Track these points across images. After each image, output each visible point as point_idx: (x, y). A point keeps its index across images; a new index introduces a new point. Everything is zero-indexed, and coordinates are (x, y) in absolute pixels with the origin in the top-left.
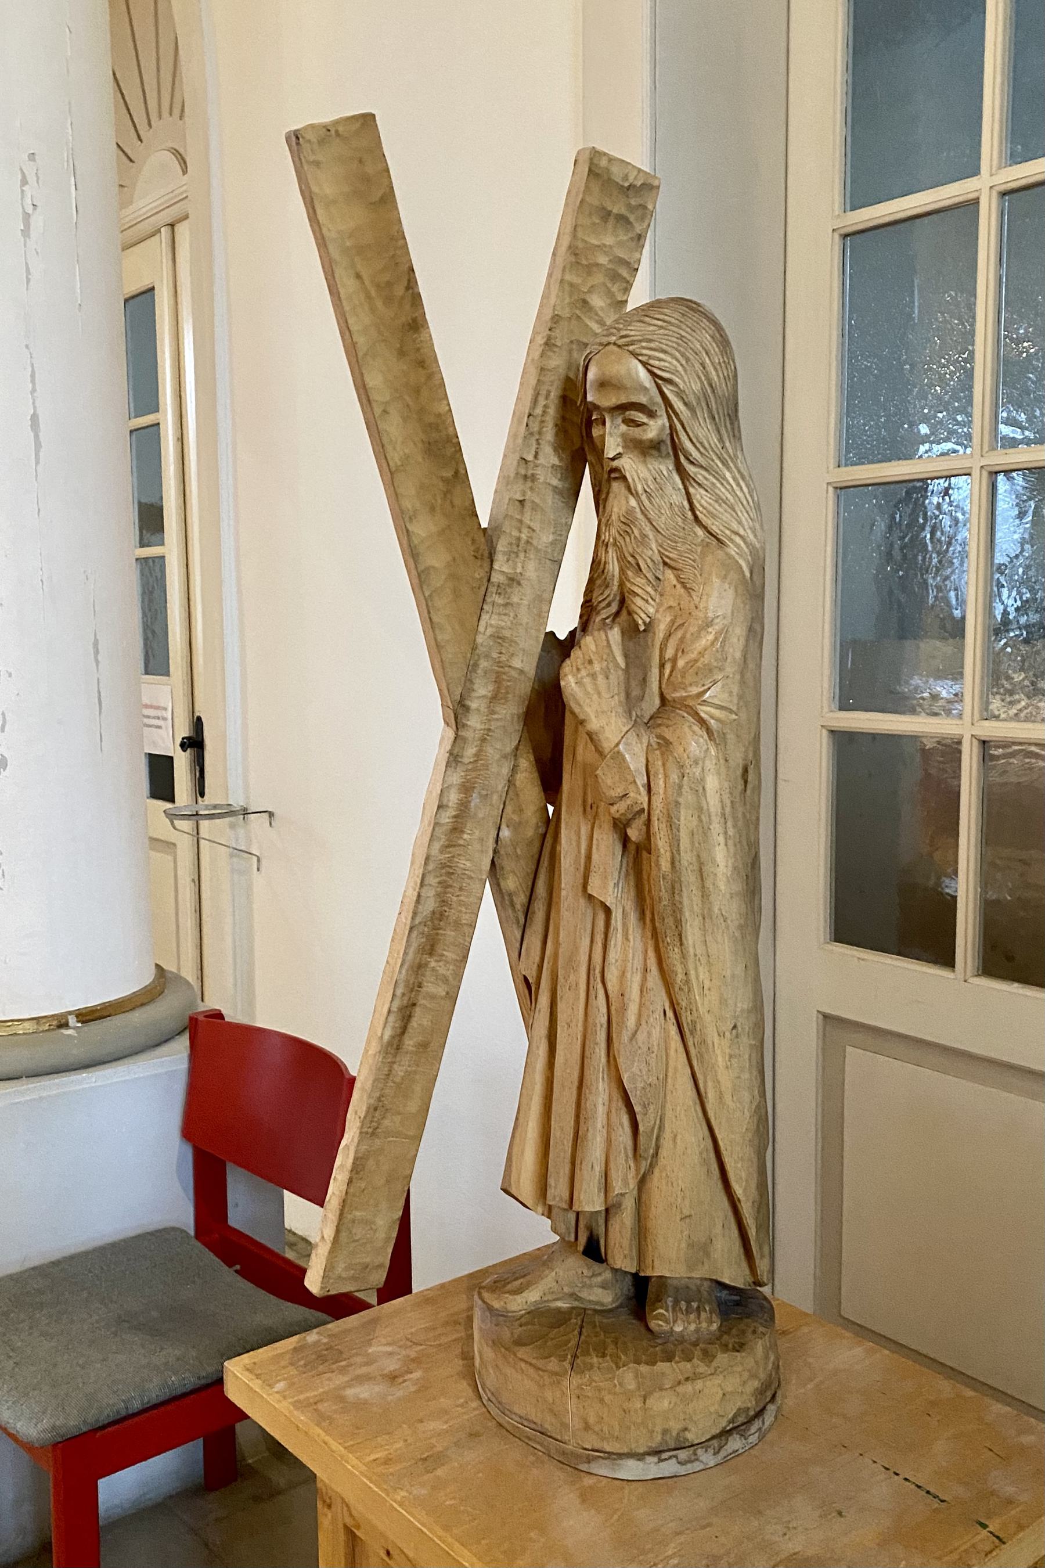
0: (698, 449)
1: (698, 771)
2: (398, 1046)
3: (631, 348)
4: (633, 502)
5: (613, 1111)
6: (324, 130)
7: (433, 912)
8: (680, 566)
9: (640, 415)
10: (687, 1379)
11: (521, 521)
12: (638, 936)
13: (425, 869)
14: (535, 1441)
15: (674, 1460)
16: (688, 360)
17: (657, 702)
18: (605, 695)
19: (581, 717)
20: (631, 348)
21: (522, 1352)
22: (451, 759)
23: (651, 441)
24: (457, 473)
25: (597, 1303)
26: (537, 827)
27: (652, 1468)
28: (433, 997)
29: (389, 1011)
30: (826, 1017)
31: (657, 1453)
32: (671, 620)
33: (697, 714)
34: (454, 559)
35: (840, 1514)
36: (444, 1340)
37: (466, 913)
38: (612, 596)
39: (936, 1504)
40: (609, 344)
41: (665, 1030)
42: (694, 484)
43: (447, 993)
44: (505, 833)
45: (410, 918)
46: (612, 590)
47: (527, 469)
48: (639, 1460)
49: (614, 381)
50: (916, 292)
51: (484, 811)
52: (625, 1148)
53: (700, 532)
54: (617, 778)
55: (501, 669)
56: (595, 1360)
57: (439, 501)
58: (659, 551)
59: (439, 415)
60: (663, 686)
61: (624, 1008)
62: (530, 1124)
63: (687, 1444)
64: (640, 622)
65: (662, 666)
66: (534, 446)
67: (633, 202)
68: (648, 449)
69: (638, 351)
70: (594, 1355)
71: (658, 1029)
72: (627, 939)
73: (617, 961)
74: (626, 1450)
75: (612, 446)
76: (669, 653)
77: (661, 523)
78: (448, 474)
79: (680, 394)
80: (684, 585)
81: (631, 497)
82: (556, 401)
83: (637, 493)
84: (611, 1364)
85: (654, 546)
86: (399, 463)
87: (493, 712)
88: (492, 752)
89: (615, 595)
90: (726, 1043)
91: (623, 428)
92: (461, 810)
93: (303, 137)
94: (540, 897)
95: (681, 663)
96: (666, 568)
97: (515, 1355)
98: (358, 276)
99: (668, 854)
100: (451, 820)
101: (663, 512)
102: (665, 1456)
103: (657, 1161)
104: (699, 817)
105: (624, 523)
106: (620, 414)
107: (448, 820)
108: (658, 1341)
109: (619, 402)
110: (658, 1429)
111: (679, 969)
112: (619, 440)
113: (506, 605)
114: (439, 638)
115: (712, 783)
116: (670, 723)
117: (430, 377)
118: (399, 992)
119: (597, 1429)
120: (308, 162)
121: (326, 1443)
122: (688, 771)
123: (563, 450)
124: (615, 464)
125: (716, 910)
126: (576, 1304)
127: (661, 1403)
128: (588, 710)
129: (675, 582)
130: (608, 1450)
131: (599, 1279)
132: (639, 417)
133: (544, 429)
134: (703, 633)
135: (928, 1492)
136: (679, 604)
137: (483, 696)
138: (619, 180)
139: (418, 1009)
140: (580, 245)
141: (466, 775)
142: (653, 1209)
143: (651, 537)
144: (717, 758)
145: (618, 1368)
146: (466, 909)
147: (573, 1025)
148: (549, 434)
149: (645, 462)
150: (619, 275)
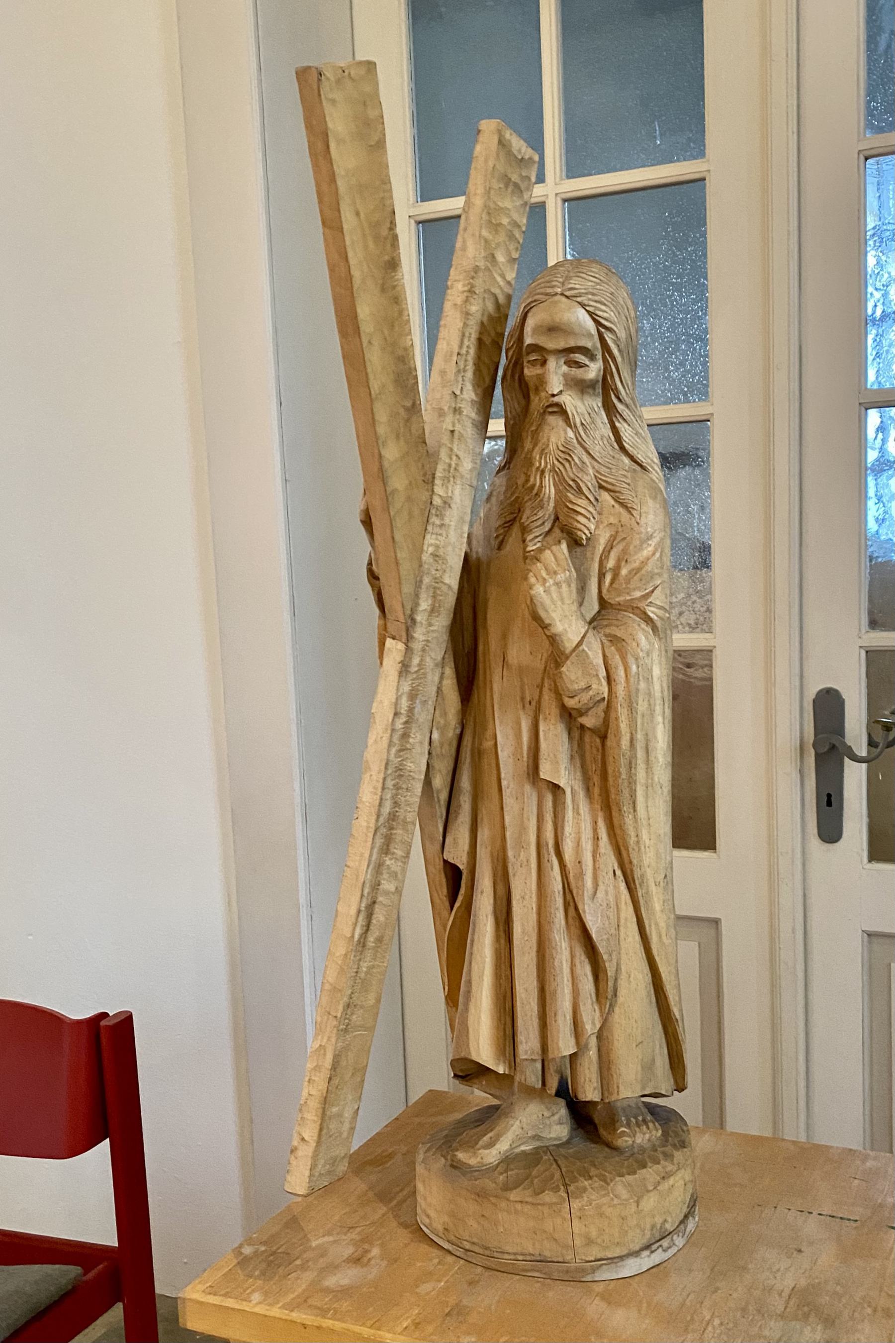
0: (625, 390)
1: (648, 661)
2: (364, 943)
3: (579, 299)
4: (571, 434)
5: (578, 964)
6: (341, 71)
7: (390, 814)
8: (617, 489)
9: (583, 357)
10: (663, 1178)
11: (451, 450)
12: (586, 809)
13: (385, 773)
15: (660, 1250)
16: (619, 313)
17: (596, 607)
18: (567, 601)
19: (547, 621)
20: (579, 299)
21: (513, 1195)
22: (403, 669)
23: (591, 380)
24: (414, 404)
25: (555, 1139)
26: (456, 728)
27: (646, 1261)
28: (387, 893)
29: (359, 911)
31: (647, 1247)
32: (611, 536)
33: (645, 613)
34: (410, 482)
35: (800, 1251)
36: (377, 1217)
37: (410, 812)
38: (547, 516)
39: (854, 1225)
40: (556, 294)
41: (616, 887)
42: (620, 420)
43: (397, 888)
44: (436, 736)
45: (373, 821)
46: (547, 510)
47: (456, 403)
48: (636, 1257)
49: (563, 327)
51: (423, 716)
52: (591, 995)
53: (626, 460)
54: (580, 673)
55: (436, 585)
56: (586, 1183)
57: (402, 429)
58: (595, 475)
59: (406, 349)
60: (604, 591)
61: (581, 875)
62: (484, 993)
63: (667, 1233)
64: (584, 537)
65: (601, 576)
66: (461, 382)
67: (524, 174)
68: (583, 387)
69: (586, 302)
70: (582, 1179)
71: (612, 887)
72: (578, 814)
73: (570, 834)
74: (625, 1252)
75: (555, 384)
76: (611, 563)
77: (596, 451)
78: (408, 404)
79: (617, 342)
80: (623, 505)
81: (569, 430)
82: (475, 343)
83: (576, 426)
84: (601, 1183)
85: (591, 471)
86: (378, 392)
87: (430, 625)
88: (429, 663)
89: (550, 515)
90: (660, 890)
91: (565, 368)
92: (409, 716)
93: (324, 75)
94: (465, 791)
95: (624, 572)
96: (602, 491)
97: (508, 1200)
98: (358, 214)
99: (628, 735)
100: (403, 726)
101: (596, 442)
102: (654, 1247)
103: (616, 1001)
104: (649, 701)
105: (562, 451)
106: (563, 357)
107: (400, 726)
108: (626, 1155)
109: (568, 346)
110: (648, 1227)
111: (633, 834)
112: (561, 378)
113: (442, 525)
114: (399, 555)
115: (656, 671)
116: (620, 623)
117: (400, 313)
118: (366, 891)
120: (326, 98)
121: (348, 1330)
122: (642, 662)
123: (478, 386)
124: (556, 399)
125: (656, 779)
126: (538, 1144)
127: (650, 1202)
128: (554, 615)
129: (613, 502)
130: (610, 1256)
131: (556, 1117)
132: (578, 358)
133: (467, 367)
134: (645, 546)
135: (841, 1218)
136: (620, 521)
137: (425, 610)
138: (516, 153)
139: (377, 906)
140: (492, 206)
141: (413, 683)
142: (615, 1042)
143: (588, 464)
144: (660, 651)
145: (608, 1184)
146: (411, 808)
148: (470, 374)
149: (582, 400)
150: (514, 236)
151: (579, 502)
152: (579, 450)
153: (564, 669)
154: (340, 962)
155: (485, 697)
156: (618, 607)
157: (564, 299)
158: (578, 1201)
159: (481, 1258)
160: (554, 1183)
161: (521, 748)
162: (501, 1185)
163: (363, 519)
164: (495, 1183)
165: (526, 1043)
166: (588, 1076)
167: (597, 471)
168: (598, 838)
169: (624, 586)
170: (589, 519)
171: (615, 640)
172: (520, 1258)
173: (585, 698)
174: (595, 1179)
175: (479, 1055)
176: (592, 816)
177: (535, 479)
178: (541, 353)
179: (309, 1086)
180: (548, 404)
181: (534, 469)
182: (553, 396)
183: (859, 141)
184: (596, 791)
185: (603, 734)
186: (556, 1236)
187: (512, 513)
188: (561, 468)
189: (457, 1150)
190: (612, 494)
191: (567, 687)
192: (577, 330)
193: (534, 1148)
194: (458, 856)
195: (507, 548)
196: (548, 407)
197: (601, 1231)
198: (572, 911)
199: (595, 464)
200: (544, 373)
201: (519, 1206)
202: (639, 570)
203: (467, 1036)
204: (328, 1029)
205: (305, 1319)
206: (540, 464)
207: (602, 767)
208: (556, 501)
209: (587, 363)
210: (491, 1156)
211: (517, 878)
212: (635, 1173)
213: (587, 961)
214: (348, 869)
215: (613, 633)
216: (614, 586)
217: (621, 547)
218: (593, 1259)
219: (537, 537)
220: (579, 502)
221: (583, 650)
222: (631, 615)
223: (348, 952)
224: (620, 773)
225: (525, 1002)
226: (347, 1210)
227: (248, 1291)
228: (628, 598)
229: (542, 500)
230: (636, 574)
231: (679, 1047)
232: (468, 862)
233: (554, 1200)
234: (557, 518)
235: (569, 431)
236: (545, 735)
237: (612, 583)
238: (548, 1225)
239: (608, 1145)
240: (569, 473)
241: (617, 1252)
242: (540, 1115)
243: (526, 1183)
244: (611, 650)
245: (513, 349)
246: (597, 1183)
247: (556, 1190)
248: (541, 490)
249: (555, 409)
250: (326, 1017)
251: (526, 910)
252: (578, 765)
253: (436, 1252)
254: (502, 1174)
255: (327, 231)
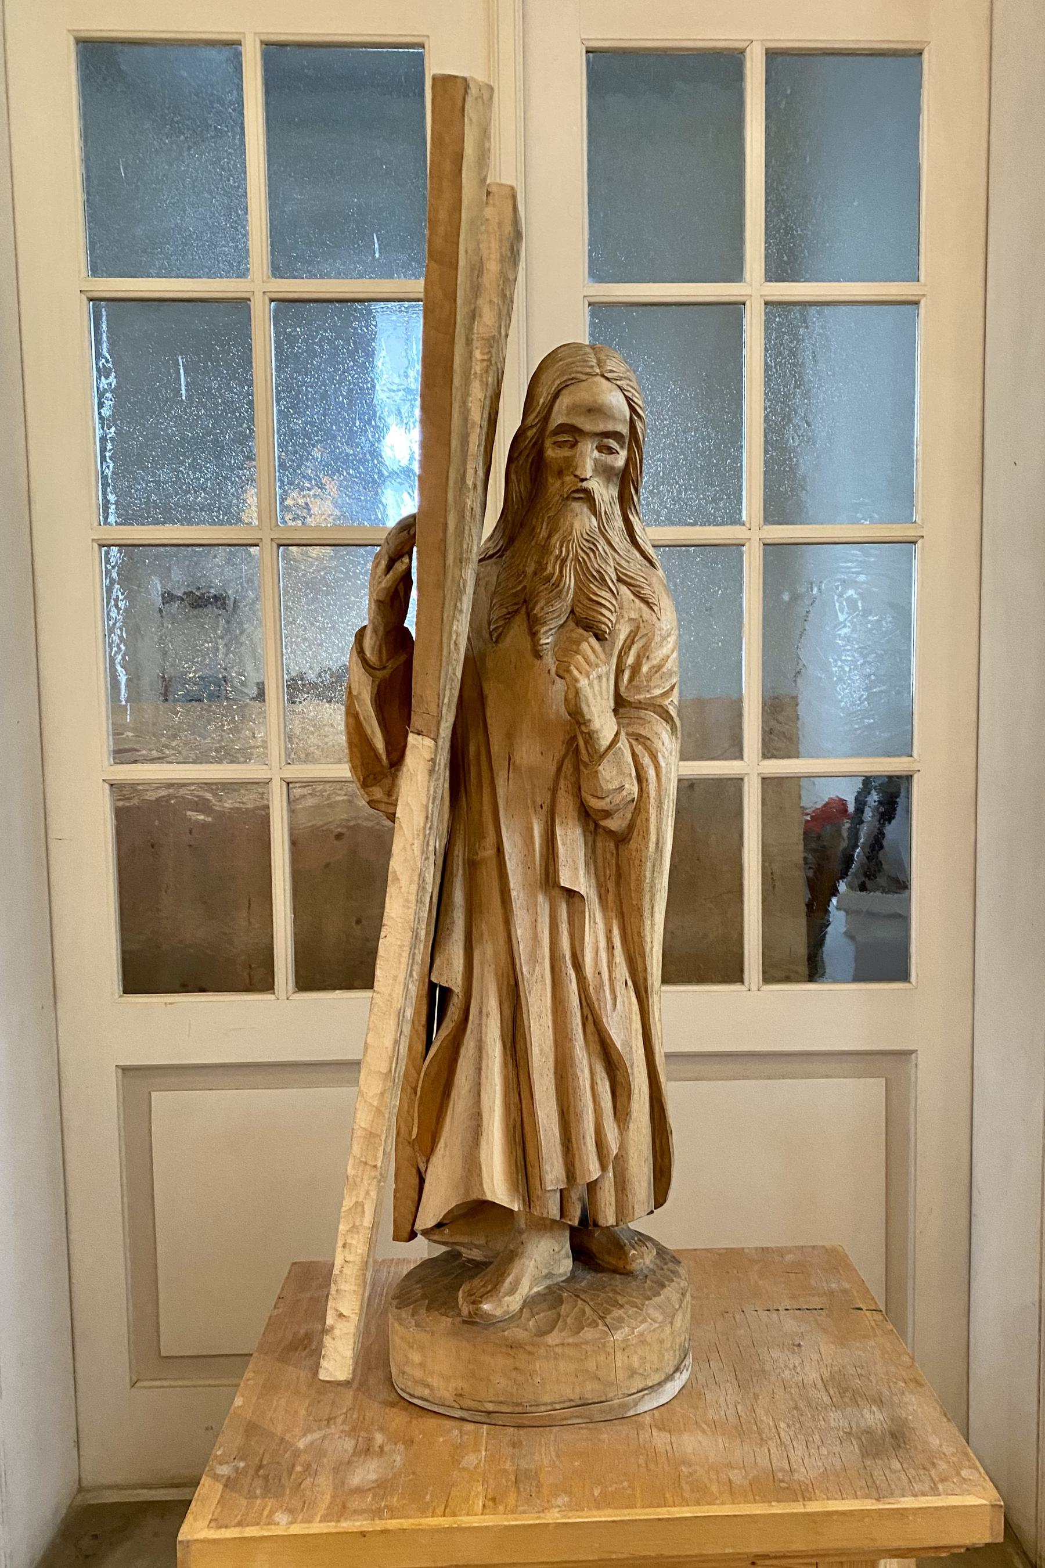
3: (618, 383)
9: (615, 444)
14: (571, 1418)
21: (552, 1339)
30: (125, 1070)
50: (182, 371)
60: (622, 689)
76: (630, 660)
91: (596, 454)
95: (645, 669)
111: (649, 940)
119: (641, 1371)
124: (585, 484)
126: (549, 1282)
129: (632, 597)
134: (665, 642)
136: (641, 617)
147: (543, 1015)
151: (603, 594)
152: (602, 541)
153: (601, 768)
154: (375, 1103)
155: (481, 802)
156: (638, 705)
157: (603, 380)
158: (619, 1332)
159: (511, 1417)
160: (588, 1318)
161: (534, 856)
162: (534, 1331)
163: (380, 599)
164: (526, 1330)
165: (552, 1171)
166: (608, 1199)
167: (618, 563)
168: (613, 947)
169: (645, 683)
170: (612, 613)
171: (638, 738)
172: (558, 1406)
173: (617, 799)
174: (627, 1306)
175: (493, 1192)
176: (606, 925)
177: (552, 567)
178: (573, 433)
179: (343, 1251)
180: (576, 488)
181: (552, 558)
182: (583, 480)
183: (584, 286)
184: (611, 897)
185: (621, 839)
186: (600, 1374)
187: (515, 604)
188: (585, 557)
189: (481, 1302)
190: (631, 588)
191: (601, 787)
192: (617, 415)
193: (547, 1287)
194: (452, 975)
195: (507, 642)
196: (574, 492)
197: (643, 1360)
198: (591, 1028)
199: (616, 556)
200: (573, 457)
201: (559, 1350)
202: (659, 667)
203: (480, 1175)
204: (365, 1182)
205: (360, 1526)
206: (561, 552)
207: (616, 871)
208: (575, 592)
209: (618, 450)
210: (513, 1303)
211: (533, 995)
212: (659, 1294)
213: (606, 1076)
214: (379, 995)
215: (637, 731)
216: (634, 683)
217: (644, 640)
218: (635, 1391)
219: (551, 629)
220: (603, 594)
221: (620, 748)
222: (652, 714)
223: (385, 1090)
224: (645, 877)
225: (548, 1129)
226: (307, 1402)
227: (266, 1513)
228: (648, 696)
229: (561, 591)
230: (656, 672)
231: (666, 1161)
232: (463, 985)
233: (598, 1336)
234: (572, 612)
235: (593, 519)
236: (562, 840)
237: (631, 679)
238: (591, 1365)
239: (615, 1271)
240: (595, 564)
241: (656, 1378)
242: (552, 1251)
243: (559, 1323)
244: (639, 749)
245: (534, 430)
246: (632, 1311)
247: (594, 1324)
248: (561, 580)
249: (582, 495)
250: (361, 1169)
251: (542, 1028)
252: (592, 871)
253: (448, 1423)
254: (529, 1320)
255: (433, 263)
